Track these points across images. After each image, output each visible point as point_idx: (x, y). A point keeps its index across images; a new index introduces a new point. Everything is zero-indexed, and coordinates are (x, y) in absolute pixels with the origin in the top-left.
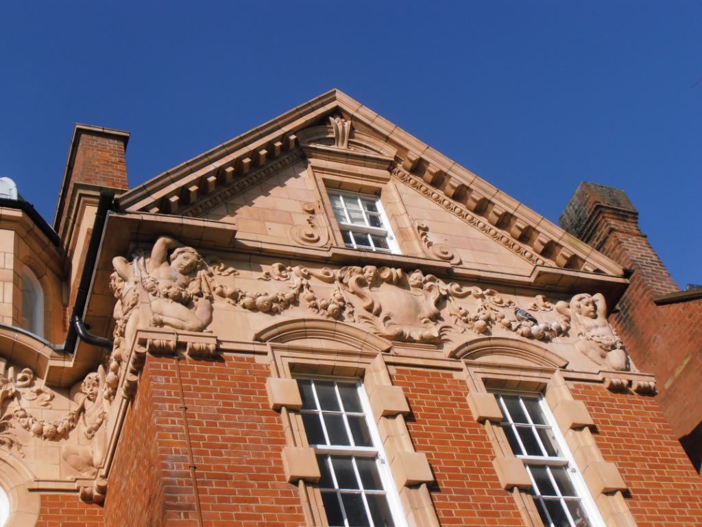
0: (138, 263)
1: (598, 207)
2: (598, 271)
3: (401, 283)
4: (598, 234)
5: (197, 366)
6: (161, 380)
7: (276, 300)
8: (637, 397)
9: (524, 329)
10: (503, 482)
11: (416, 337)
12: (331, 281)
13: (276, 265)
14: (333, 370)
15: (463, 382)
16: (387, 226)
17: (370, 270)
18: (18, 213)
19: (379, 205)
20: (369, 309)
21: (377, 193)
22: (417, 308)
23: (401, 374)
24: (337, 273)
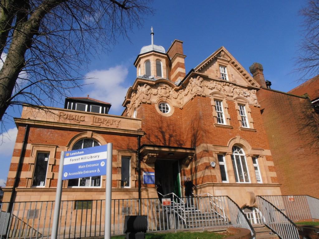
0: (195, 79)
1: (257, 68)
2: (257, 86)
3: (229, 86)
4: (256, 73)
5: (202, 98)
6: (198, 100)
7: (212, 88)
8: (257, 108)
9: (244, 95)
10: (238, 120)
11: (230, 95)
12: (219, 84)
13: (212, 81)
14: (218, 100)
15: (235, 103)
16: (226, 73)
17: (225, 83)
18: (166, 56)
19: (226, 68)
20: (224, 90)
21: (226, 67)
22: (230, 90)
23: (229, 102)
24: (220, 83)
